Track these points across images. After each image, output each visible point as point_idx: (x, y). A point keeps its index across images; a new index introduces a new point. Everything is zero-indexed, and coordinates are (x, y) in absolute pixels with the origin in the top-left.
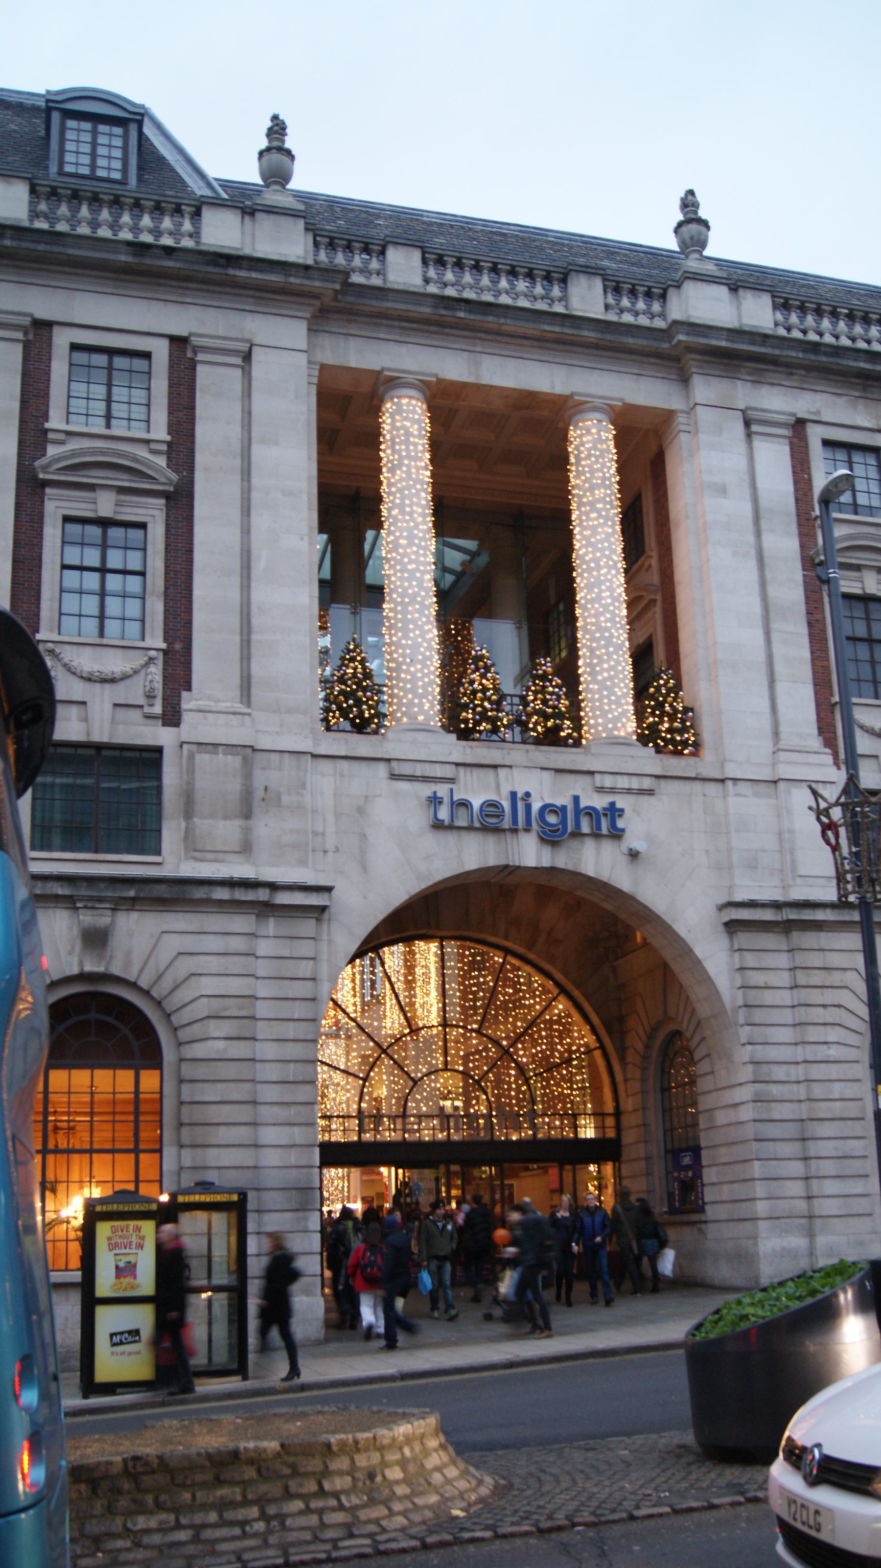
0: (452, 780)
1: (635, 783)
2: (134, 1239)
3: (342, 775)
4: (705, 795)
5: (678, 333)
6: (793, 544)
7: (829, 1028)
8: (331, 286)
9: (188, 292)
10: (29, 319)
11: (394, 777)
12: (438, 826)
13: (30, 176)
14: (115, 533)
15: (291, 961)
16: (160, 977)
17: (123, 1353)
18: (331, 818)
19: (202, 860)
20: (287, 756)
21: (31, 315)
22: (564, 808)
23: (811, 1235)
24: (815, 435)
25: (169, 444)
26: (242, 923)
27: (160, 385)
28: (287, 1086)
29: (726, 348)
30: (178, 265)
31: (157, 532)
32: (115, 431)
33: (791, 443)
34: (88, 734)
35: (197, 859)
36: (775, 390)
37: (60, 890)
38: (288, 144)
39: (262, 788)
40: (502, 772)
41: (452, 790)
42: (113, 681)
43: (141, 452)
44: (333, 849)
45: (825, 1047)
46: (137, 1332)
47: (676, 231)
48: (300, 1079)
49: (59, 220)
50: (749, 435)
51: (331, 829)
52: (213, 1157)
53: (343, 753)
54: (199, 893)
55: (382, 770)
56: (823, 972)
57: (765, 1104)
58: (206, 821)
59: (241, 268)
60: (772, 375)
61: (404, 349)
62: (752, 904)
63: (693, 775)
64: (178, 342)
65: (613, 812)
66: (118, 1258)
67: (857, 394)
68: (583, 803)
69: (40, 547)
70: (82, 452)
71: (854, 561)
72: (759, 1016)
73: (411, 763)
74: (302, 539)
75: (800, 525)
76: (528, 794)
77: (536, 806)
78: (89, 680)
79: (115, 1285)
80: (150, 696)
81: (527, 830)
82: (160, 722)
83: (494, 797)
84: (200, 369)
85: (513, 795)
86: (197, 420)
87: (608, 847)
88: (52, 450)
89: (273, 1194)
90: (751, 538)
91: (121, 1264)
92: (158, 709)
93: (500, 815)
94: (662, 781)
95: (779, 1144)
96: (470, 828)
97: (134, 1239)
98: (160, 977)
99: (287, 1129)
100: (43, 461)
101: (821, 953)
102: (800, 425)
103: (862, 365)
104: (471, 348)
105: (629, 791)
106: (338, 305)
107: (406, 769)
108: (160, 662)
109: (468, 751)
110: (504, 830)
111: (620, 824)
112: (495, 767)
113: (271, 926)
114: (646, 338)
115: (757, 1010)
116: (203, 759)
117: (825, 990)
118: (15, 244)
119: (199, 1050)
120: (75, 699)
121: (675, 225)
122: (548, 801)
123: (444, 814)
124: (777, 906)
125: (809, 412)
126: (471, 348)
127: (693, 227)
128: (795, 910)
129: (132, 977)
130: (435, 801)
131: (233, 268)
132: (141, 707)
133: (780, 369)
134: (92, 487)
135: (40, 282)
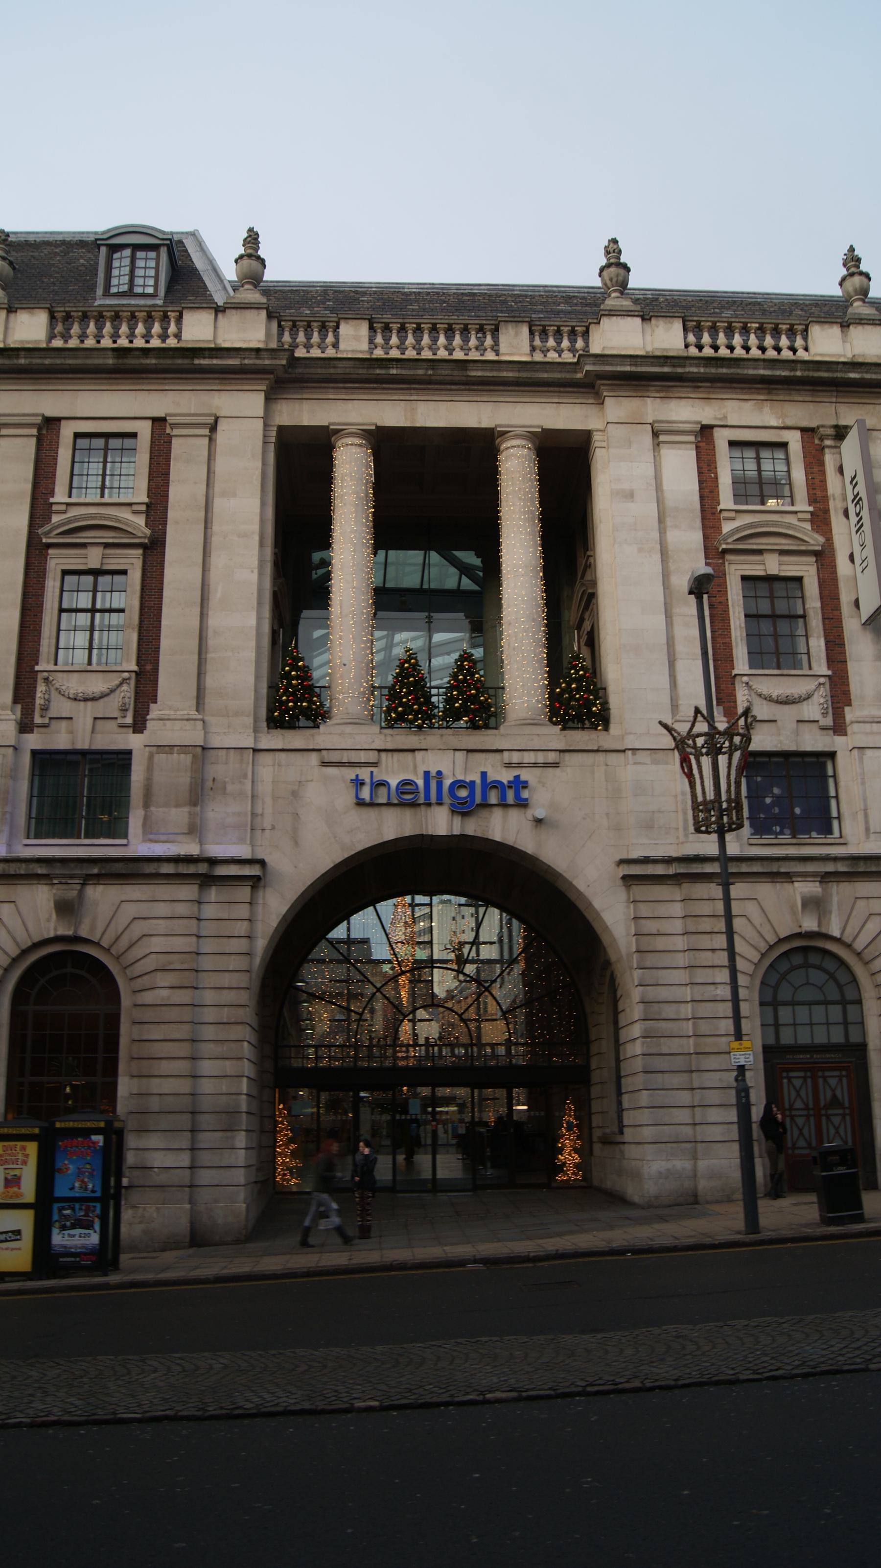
0: (375, 764)
1: (541, 758)
2: (20, 1157)
3: (279, 765)
4: (607, 765)
5: (585, 364)
6: (697, 537)
7: (717, 969)
8: (278, 362)
9: (167, 381)
10: (41, 418)
11: (325, 764)
12: (361, 803)
13: (48, 306)
14: (104, 580)
15: (228, 922)
16: (118, 938)
17: (7, 1249)
18: (269, 801)
19: (156, 842)
20: (232, 751)
21: (43, 415)
22: (473, 783)
23: (695, 1158)
24: (721, 438)
25: (148, 505)
26: (189, 891)
27: (143, 457)
28: (221, 1026)
29: (631, 372)
30: (154, 361)
31: (135, 576)
32: (107, 499)
33: (697, 447)
34: (73, 744)
35: (152, 841)
36: (683, 402)
37: (40, 870)
38: (261, 253)
39: (211, 779)
40: (419, 755)
41: (372, 773)
42: (94, 699)
43: (125, 514)
44: (270, 827)
45: (712, 987)
46: (18, 1232)
47: (841, 284)
48: (233, 1020)
49: (392, 348)
50: (657, 445)
51: (269, 810)
52: (157, 1086)
53: (280, 747)
54: (150, 869)
55: (314, 758)
56: (712, 919)
57: (655, 1039)
58: (161, 809)
59: (204, 358)
60: (680, 389)
61: (350, 405)
62: (646, 861)
63: (595, 748)
64: (158, 422)
65: (518, 784)
66: (7, 1171)
67: (762, 397)
68: (489, 780)
69: (42, 595)
70: (76, 519)
71: (755, 547)
72: (650, 960)
73: (339, 752)
74: (252, 572)
75: (703, 519)
76: (439, 773)
77: (447, 783)
78: (75, 699)
79: (4, 1193)
80: (124, 710)
81: (439, 803)
82: (131, 730)
83: (411, 777)
84: (175, 441)
85: (427, 774)
86: (171, 483)
87: (514, 814)
88: (55, 519)
89: (207, 1116)
90: (656, 535)
91: (9, 1177)
92: (129, 720)
93: (416, 792)
94: (567, 755)
95: (666, 1075)
96: (389, 804)
97: (20, 1157)
98: (118, 938)
99: (220, 1062)
100: (47, 528)
101: (711, 902)
102: (705, 431)
103: (762, 372)
104: (408, 398)
105: (535, 765)
106: (289, 376)
107: (335, 757)
108: (133, 682)
109: (389, 738)
110: (419, 805)
111: (525, 794)
112: (413, 751)
113: (213, 893)
114: (560, 372)
115: (649, 955)
116: (161, 759)
117: (714, 935)
118: (399, 372)
119: (148, 998)
120: (64, 716)
121: (839, 279)
122: (460, 777)
123: (365, 793)
124: (668, 861)
125: (716, 419)
126: (408, 398)
127: (857, 279)
128: (682, 865)
129: (95, 939)
130: (358, 783)
131: (198, 358)
132: (116, 718)
133: (685, 384)
134: (83, 546)
135: (315, 397)
